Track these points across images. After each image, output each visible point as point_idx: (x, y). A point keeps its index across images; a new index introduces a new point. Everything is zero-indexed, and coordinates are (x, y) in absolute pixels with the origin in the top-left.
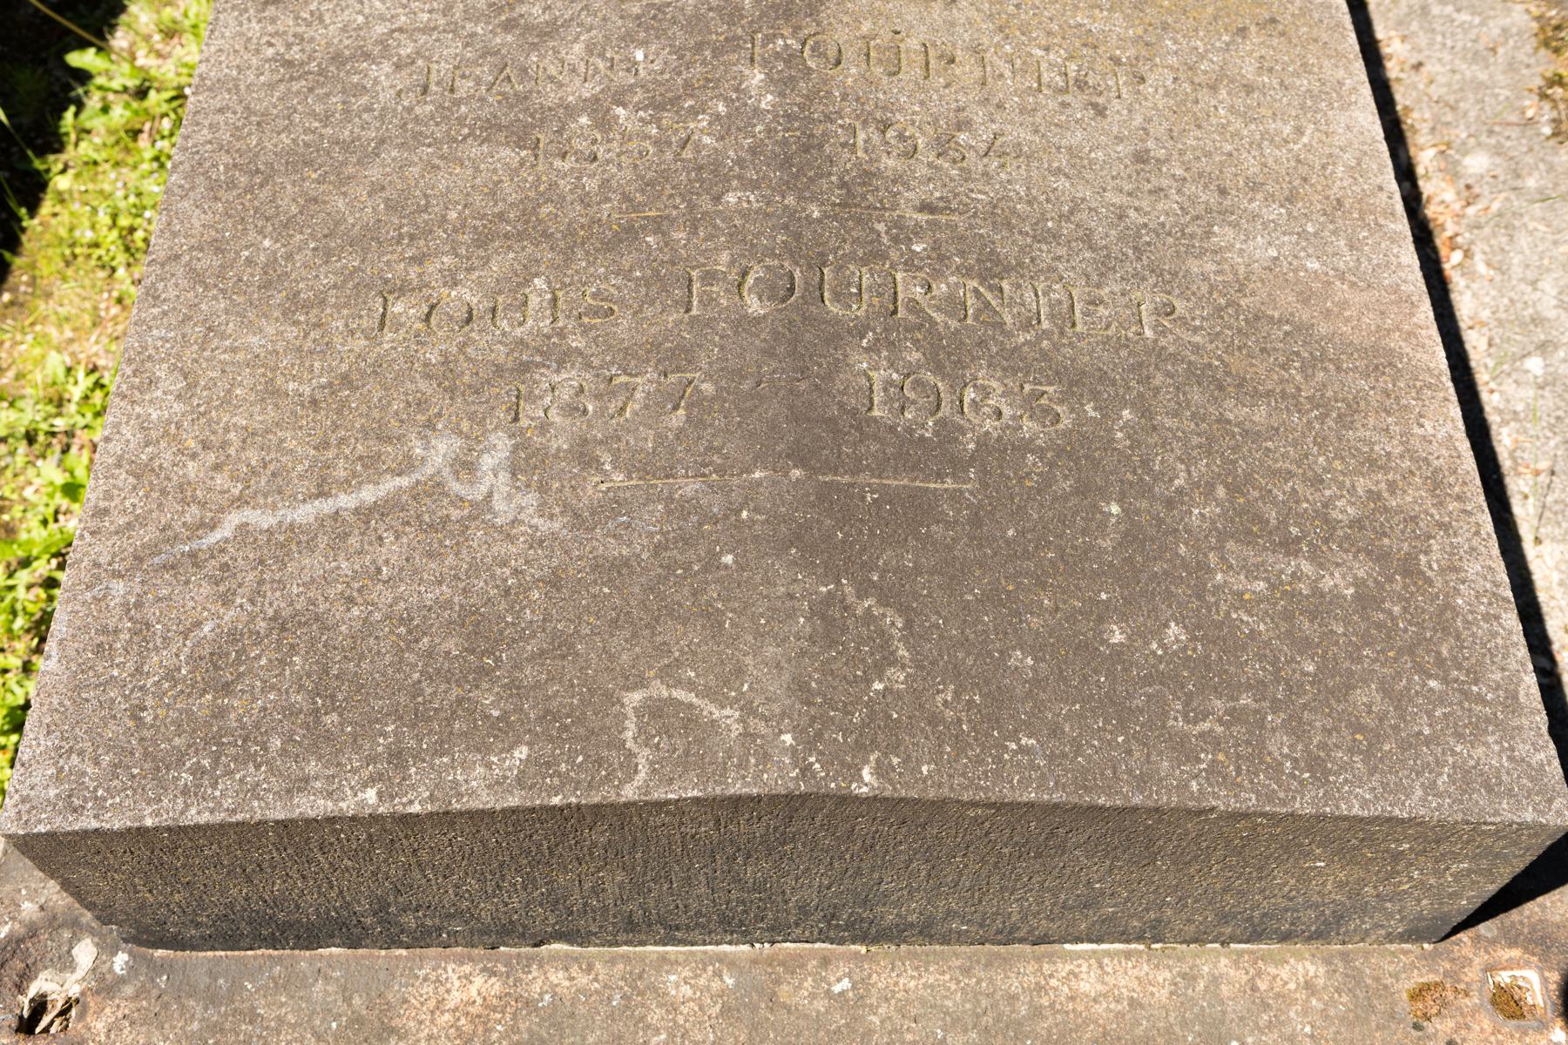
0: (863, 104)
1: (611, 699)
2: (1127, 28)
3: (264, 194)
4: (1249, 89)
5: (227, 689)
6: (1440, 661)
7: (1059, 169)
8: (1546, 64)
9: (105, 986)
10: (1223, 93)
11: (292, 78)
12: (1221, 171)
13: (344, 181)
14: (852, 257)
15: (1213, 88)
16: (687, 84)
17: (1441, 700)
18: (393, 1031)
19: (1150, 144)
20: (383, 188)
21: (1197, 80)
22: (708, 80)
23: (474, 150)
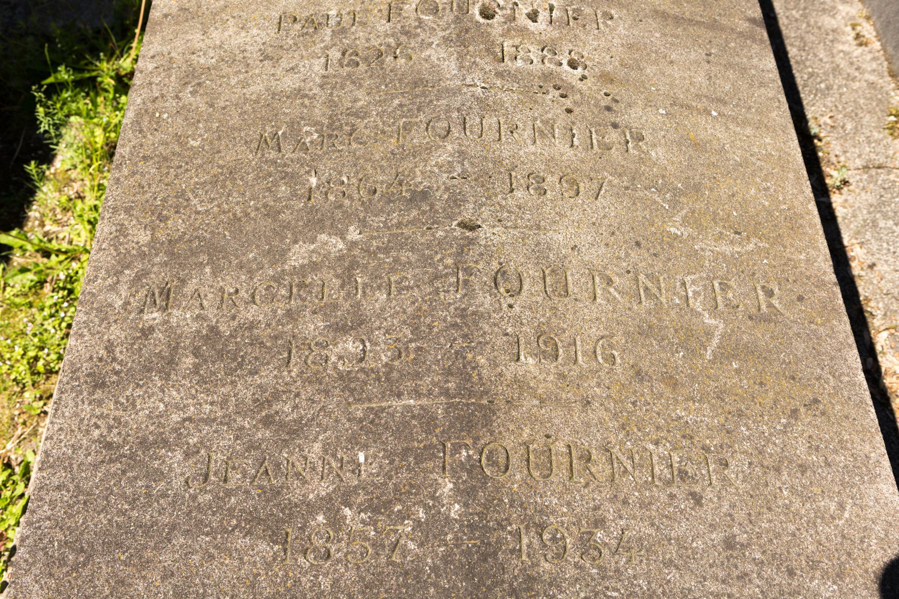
0: (525, 509)
2: (713, 418)
4: (803, 468)
7: (671, 561)
10: (785, 476)
11: (111, 461)
12: (788, 552)
15: (778, 470)
19: (736, 530)
20: (172, 575)
21: (766, 463)
22: (411, 486)
23: (241, 542)
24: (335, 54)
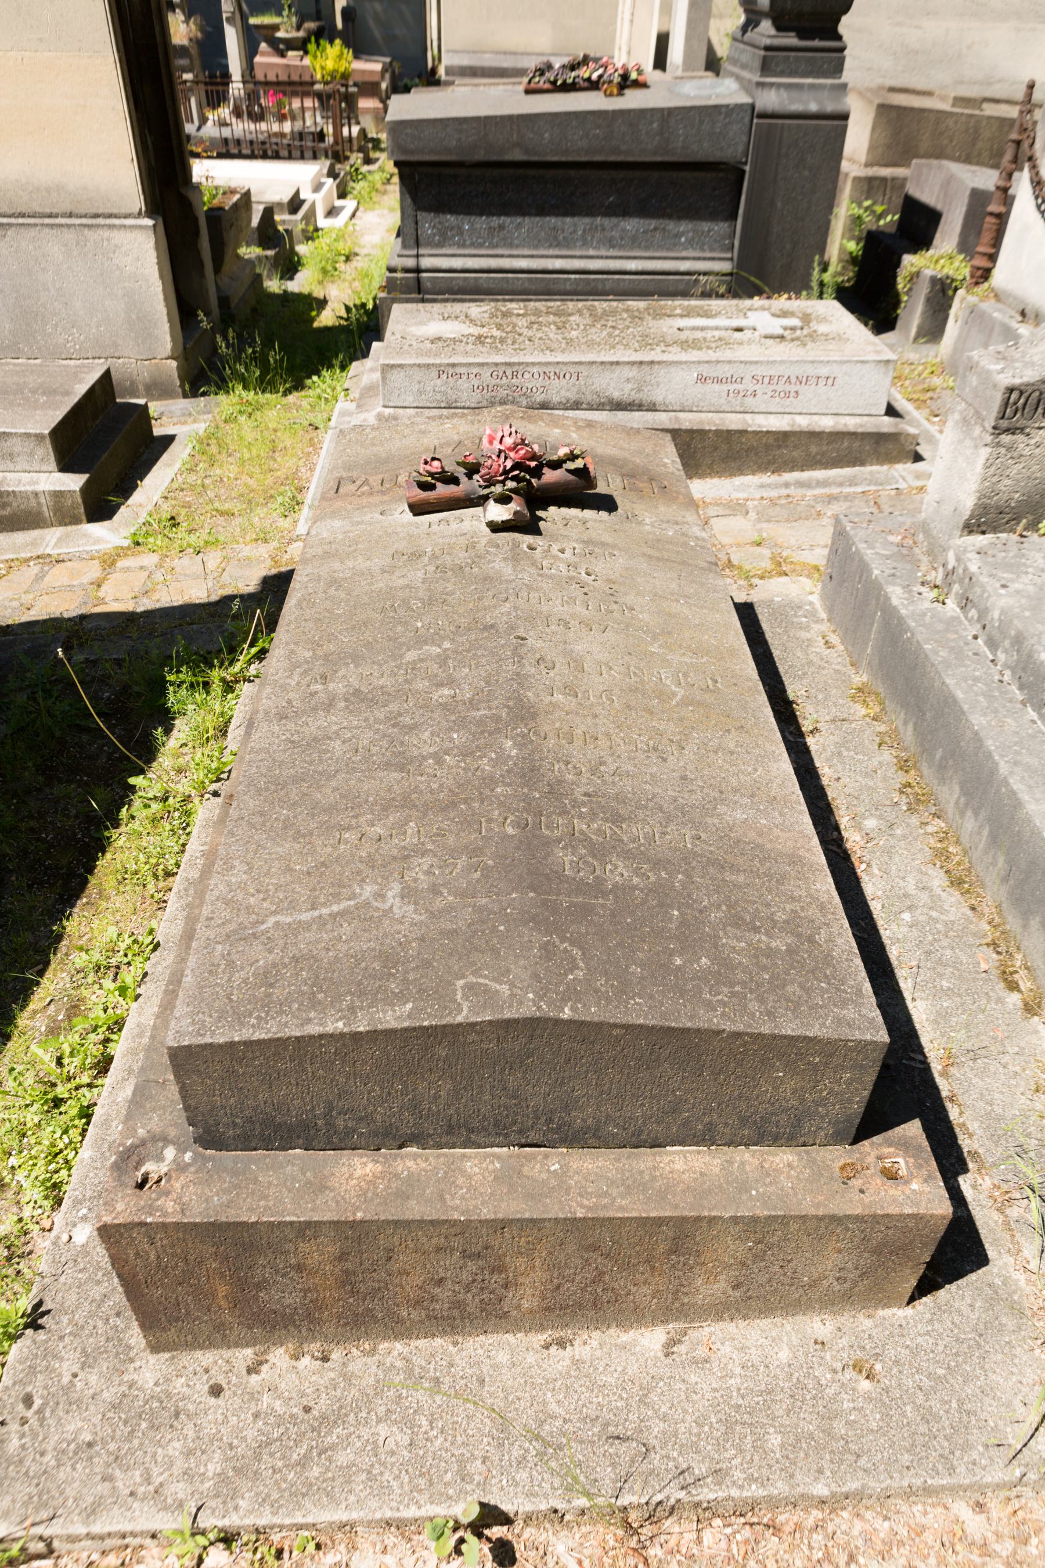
1: (450, 983)
3: (283, 793)
4: (732, 753)
5: (272, 986)
6: (826, 976)
8: (902, 778)
9: (180, 1167)
13: (319, 787)
14: (554, 813)
15: (716, 752)
16: (477, 747)
17: (827, 991)
18: (327, 1188)
23: (380, 774)
24: (431, 568)
